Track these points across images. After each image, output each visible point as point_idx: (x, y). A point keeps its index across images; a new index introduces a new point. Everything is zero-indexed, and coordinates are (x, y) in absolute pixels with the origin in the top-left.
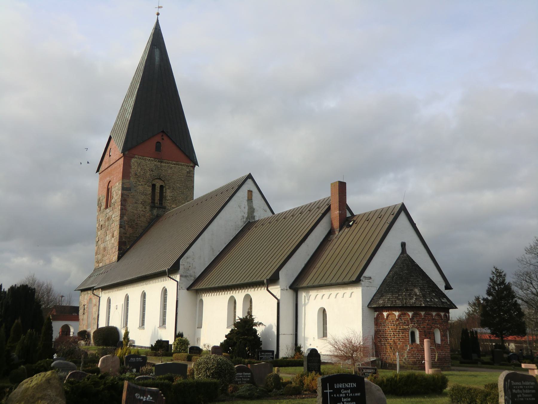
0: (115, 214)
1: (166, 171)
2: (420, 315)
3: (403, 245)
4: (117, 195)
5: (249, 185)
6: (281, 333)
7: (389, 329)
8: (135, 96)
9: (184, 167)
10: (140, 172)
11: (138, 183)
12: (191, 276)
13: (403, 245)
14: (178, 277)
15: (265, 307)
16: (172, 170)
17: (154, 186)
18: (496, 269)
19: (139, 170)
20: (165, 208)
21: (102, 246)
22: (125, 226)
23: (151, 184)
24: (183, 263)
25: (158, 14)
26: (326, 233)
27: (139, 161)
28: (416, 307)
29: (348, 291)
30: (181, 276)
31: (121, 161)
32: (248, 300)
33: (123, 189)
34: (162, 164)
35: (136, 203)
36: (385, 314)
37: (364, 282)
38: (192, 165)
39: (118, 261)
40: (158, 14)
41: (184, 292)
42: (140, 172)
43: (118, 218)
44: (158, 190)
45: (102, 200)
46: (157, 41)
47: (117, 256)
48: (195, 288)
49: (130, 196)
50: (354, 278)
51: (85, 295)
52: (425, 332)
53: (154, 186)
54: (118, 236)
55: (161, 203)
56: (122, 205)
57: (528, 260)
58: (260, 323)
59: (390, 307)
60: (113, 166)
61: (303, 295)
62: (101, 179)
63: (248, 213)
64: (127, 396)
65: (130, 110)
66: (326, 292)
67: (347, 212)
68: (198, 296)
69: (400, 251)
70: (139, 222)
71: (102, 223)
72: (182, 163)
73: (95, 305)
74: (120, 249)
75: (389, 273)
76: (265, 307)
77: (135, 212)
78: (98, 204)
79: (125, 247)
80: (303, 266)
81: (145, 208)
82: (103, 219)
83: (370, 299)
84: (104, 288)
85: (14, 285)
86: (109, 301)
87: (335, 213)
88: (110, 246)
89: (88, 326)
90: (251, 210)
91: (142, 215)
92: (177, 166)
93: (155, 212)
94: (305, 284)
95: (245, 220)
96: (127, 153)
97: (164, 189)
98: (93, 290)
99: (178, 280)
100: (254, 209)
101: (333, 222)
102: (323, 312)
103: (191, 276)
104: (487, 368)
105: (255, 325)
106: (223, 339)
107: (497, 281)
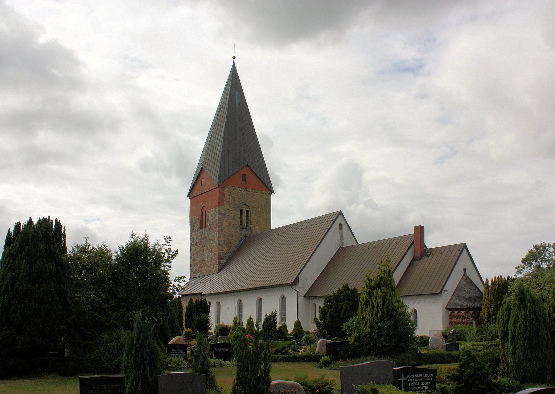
0: (213, 235)
5: (340, 220)
17: (241, 211)
25: (234, 58)
34: (247, 193)
35: (229, 225)
36: (456, 312)
38: (269, 192)
40: (234, 58)
46: (234, 85)
50: (438, 292)
53: (241, 211)
55: (247, 226)
60: (207, 194)
64: (85, 379)
70: (232, 241)
81: (236, 229)
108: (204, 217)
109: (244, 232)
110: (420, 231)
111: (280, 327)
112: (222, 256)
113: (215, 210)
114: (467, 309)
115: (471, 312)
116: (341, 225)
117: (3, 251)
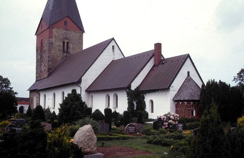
3: (188, 73)
5: (113, 43)
10: (57, 36)
13: (188, 73)
16: (72, 35)
17: (64, 42)
19: (57, 34)
20: (69, 53)
23: (62, 42)
34: (68, 32)
36: (180, 103)
38: (82, 32)
44: (66, 44)
50: (167, 88)
53: (64, 42)
67: (162, 57)
69: (187, 75)
72: (77, 32)
97: (69, 43)
109: (65, 54)
110: (158, 46)
111: (113, 112)
112: (50, 67)
114: (188, 101)
115: (192, 103)
116: (113, 47)
117: (138, 86)
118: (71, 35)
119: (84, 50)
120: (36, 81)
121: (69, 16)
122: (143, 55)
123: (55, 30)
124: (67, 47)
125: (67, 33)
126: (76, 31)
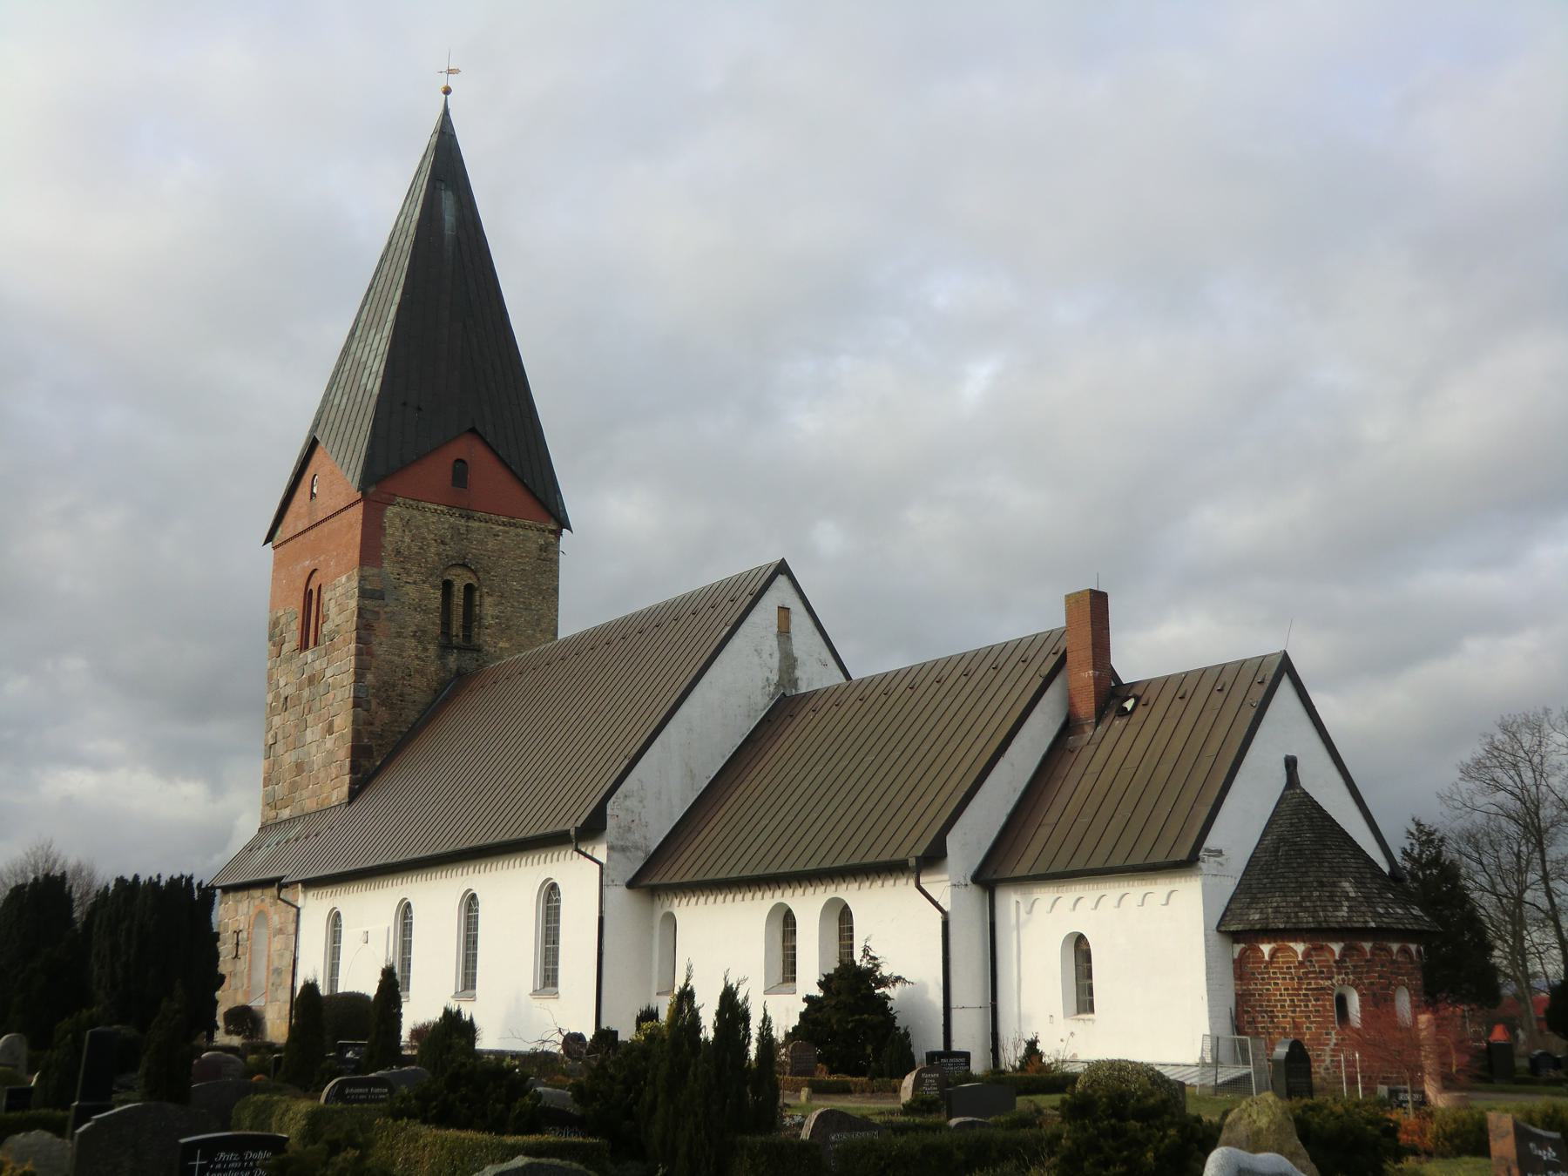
0: (337, 668)
1: (481, 542)
2: (1361, 951)
3: (1291, 764)
4: (341, 611)
5: (780, 592)
6: (954, 1002)
7: (1279, 990)
8: (389, 325)
9: (530, 533)
10: (409, 547)
11: (404, 578)
12: (637, 848)
13: (1291, 764)
14: (601, 852)
15: (901, 931)
16: (499, 540)
17: (447, 586)
18: (1418, 824)
19: (407, 540)
20: (479, 650)
21: (289, 759)
22: (369, 702)
23: (439, 582)
24: (616, 812)
25: (447, 91)
26: (1054, 729)
27: (406, 514)
28: (1347, 929)
29: (1158, 889)
30: (611, 848)
31: (357, 513)
32: (843, 917)
33: (363, 594)
35: (399, 635)
36: (1266, 949)
37: (1207, 864)
38: (552, 526)
39: (350, 803)
40: (447, 91)
41: (618, 895)
42: (409, 547)
43: (348, 679)
44: (458, 599)
45: (288, 624)
46: (445, 168)
47: (345, 789)
48: (655, 881)
49: (383, 616)
50: (1183, 854)
51: (237, 902)
52: (1374, 995)
53: (447, 586)
54: (348, 731)
55: (468, 637)
56: (359, 639)
57: (1465, 795)
58: (898, 979)
59: (1284, 930)
61: (1011, 902)
62: (278, 564)
63: (780, 670)
65: (377, 366)
66: (1087, 893)
68: (658, 903)
70: (408, 690)
71: (284, 692)
72: (527, 522)
73: (281, 931)
74: (354, 768)
75: (1261, 840)
76: (901, 931)
77: (397, 660)
78: (271, 637)
79: (370, 762)
80: (1003, 820)
81: (425, 650)
82: (292, 679)
83: (1222, 909)
84: (311, 884)
85: (129, 877)
86: (335, 919)
87: (1083, 675)
88: (317, 758)
89: (247, 994)
90: (788, 663)
91: (417, 671)
92: (513, 531)
93: (452, 660)
94: (1020, 871)
95: (772, 689)
96: (372, 490)
98: (282, 886)
99: (604, 860)
100: (795, 660)
101: (1077, 700)
102: (1080, 948)
103: (637, 848)
104: (1503, 1091)
105: (883, 982)
106: (796, 1021)
107: (1420, 855)
108: (314, 607)
113: (349, 579)
116: (784, 611)
118: (491, 544)
119: (568, 642)
120: (263, 828)
121: (479, 429)
122: (1019, 653)
123: (398, 514)
124: (468, 625)
125: (468, 529)
126: (521, 522)
